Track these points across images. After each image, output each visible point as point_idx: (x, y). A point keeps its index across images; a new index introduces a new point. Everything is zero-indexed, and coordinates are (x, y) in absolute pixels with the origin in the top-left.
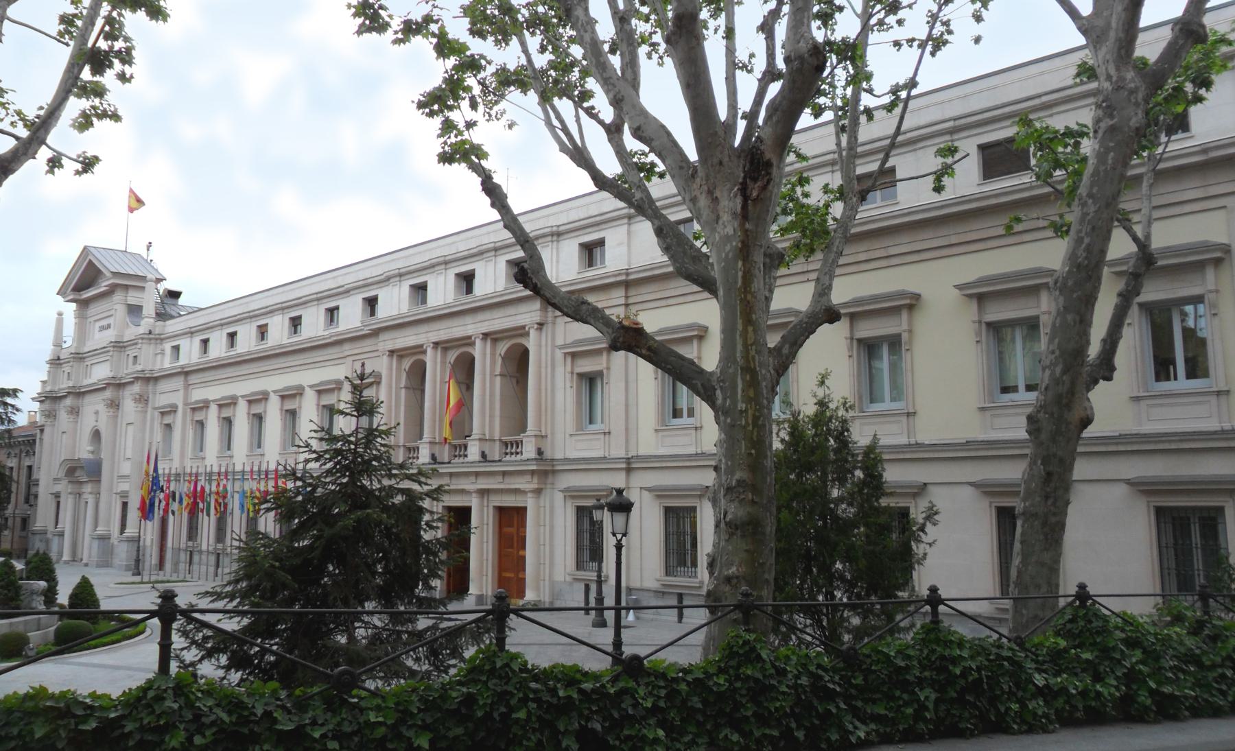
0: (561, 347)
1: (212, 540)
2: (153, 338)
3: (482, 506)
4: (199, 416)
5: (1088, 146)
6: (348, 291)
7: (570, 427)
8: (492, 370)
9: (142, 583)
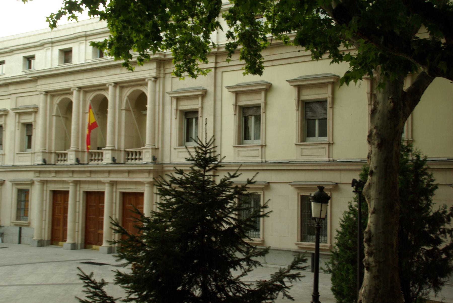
0: (169, 93)
6: (12, 51)
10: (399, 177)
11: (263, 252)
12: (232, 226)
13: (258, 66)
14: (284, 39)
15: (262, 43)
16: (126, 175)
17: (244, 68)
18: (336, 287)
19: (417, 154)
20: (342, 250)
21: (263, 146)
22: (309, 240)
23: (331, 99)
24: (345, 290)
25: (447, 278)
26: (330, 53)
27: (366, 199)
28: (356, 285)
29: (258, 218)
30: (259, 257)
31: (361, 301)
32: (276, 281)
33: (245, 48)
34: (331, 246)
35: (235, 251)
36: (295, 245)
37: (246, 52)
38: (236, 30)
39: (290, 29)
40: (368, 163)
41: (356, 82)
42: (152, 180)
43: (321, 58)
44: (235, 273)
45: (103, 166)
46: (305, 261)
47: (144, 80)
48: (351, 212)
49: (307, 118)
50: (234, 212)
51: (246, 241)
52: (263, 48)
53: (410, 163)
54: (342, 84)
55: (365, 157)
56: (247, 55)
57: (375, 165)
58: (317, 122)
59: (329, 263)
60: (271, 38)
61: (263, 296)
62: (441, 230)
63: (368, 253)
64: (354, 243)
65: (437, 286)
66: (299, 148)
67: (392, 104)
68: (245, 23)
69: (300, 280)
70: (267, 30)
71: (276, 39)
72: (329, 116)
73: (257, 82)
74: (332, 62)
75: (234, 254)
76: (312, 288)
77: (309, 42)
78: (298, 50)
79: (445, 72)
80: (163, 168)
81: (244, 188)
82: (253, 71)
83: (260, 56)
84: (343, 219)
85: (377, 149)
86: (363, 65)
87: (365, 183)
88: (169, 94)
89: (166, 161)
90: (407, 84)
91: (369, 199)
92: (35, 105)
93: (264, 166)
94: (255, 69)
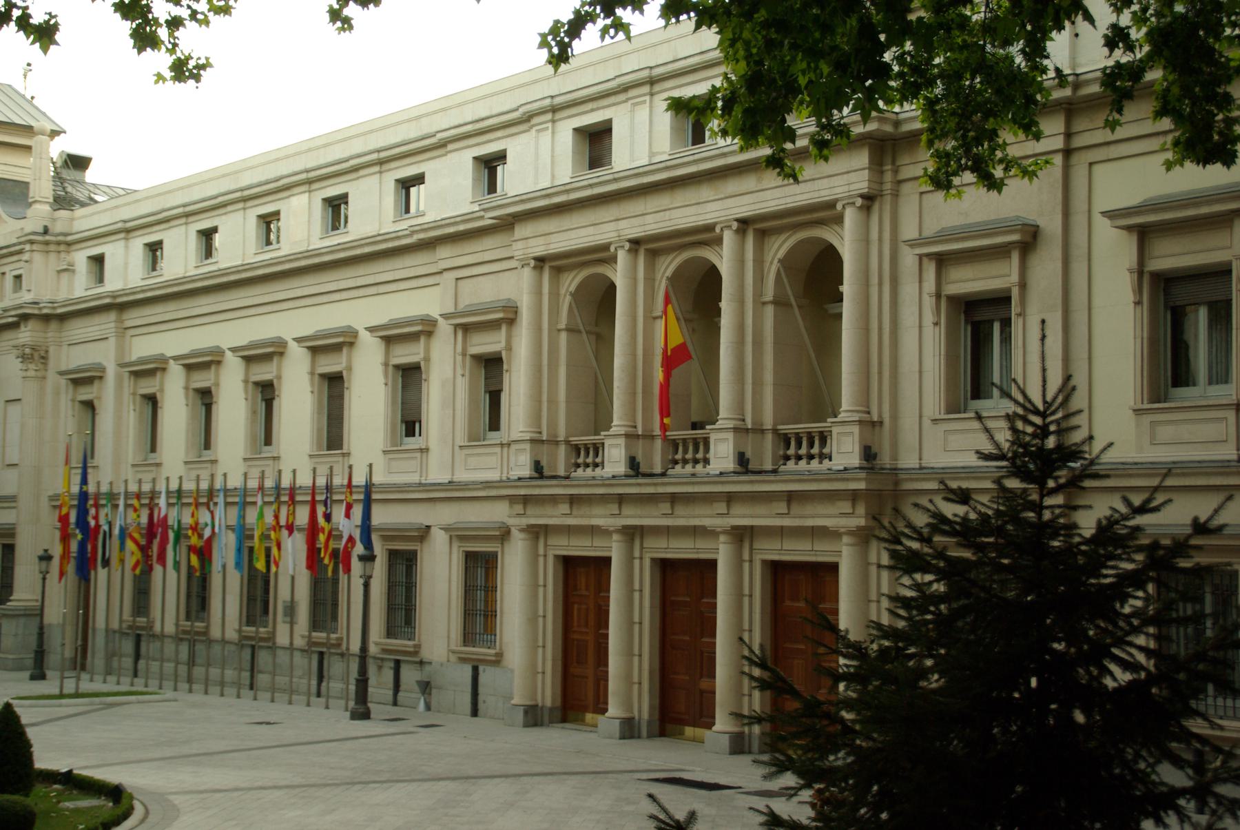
0: (912, 244)
1: (127, 615)
2: (52, 242)
3: (629, 559)
4: (147, 386)
5: (1016, 53)
6: (442, 145)
7: (934, 401)
8: (758, 293)
9: (62, 696)
13: (1220, 133)
16: (782, 507)
17: (1168, 145)
37: (1176, 90)
42: (862, 522)
45: (604, 482)
47: (831, 205)
51: (1195, 730)
56: (1179, 100)
73: (1217, 187)
75: (1154, 772)
80: (897, 483)
81: (1181, 547)
88: (912, 246)
89: (908, 460)
92: (350, 327)
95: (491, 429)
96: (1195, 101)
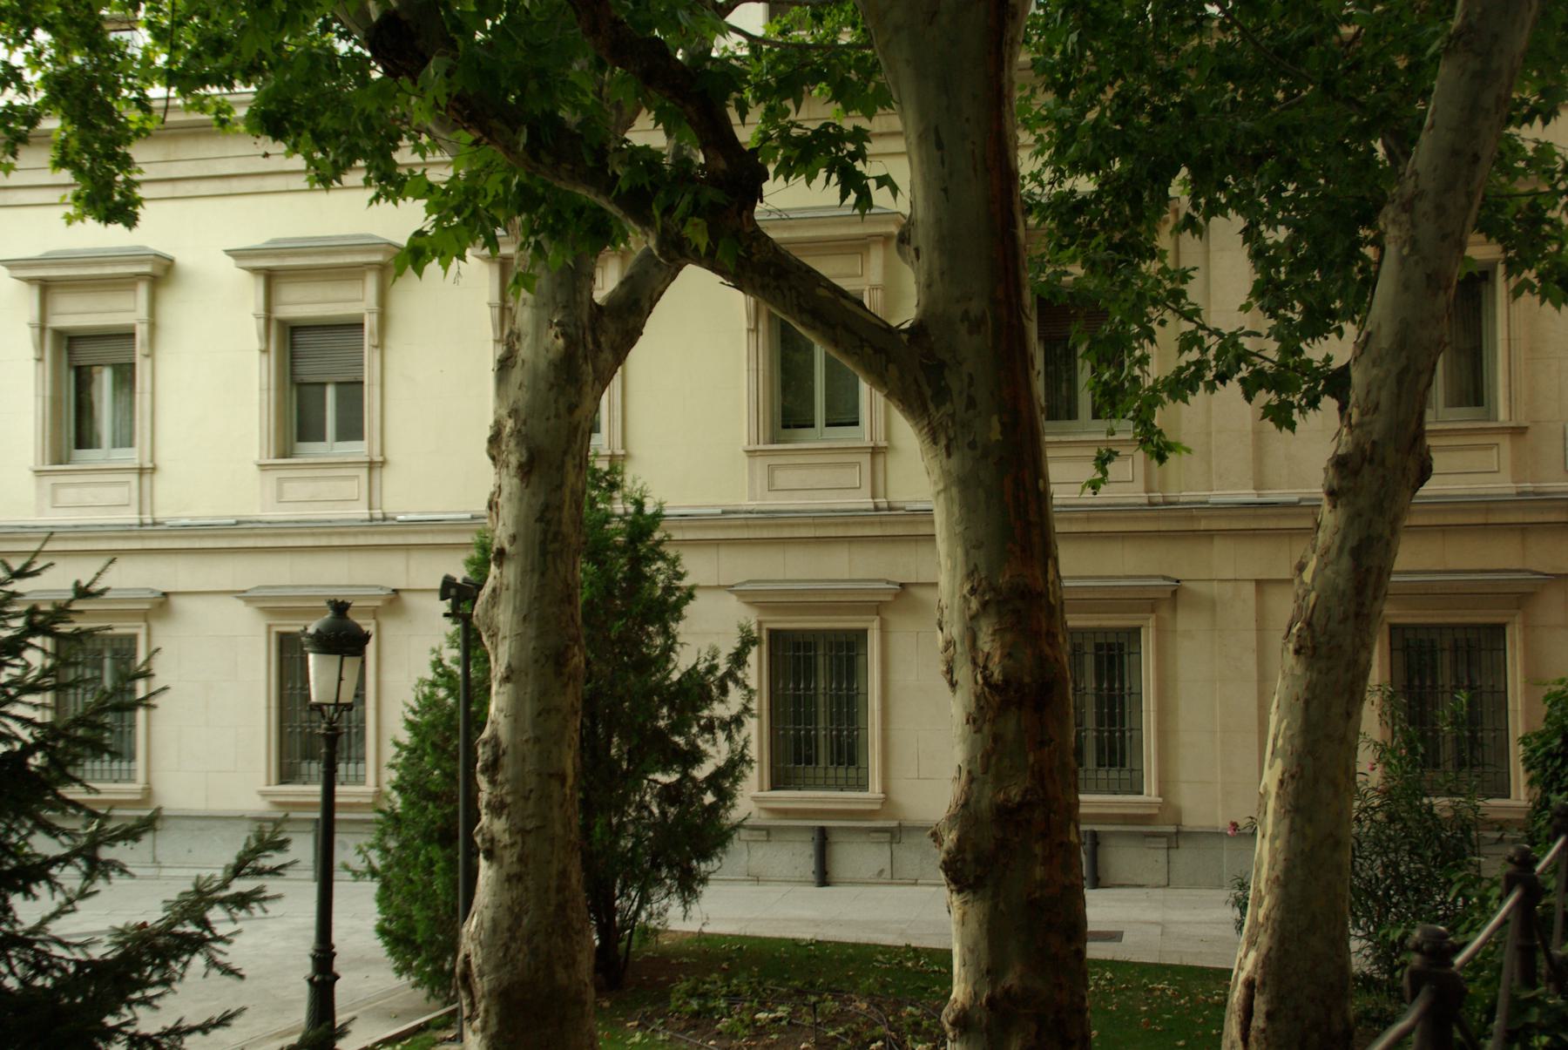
10: (585, 569)
11: (133, 827)
12: (18, 746)
13: (121, 194)
14: (214, 109)
15: (134, 115)
17: (69, 200)
18: (391, 921)
19: (637, 496)
20: (410, 804)
21: (374, 465)
22: (305, 778)
23: (374, 318)
24: (421, 927)
25: (716, 861)
26: (369, 169)
27: (485, 638)
28: (455, 910)
29: (127, 714)
30: (121, 844)
31: (467, 956)
32: (180, 921)
33: (69, 129)
34: (379, 794)
35: (31, 833)
36: (258, 798)
37: (74, 143)
38: (35, 61)
39: (232, 78)
40: (490, 525)
41: (446, 267)
43: (340, 182)
44: (27, 911)
46: (281, 846)
48: (440, 681)
49: (298, 379)
50: (27, 698)
51: (70, 797)
52: (137, 134)
53: (615, 524)
54: (400, 273)
55: (481, 507)
56: (78, 153)
57: (511, 531)
58: (330, 393)
59: (372, 847)
60: (163, 103)
61: (135, 975)
62: (702, 722)
63: (488, 805)
64: (450, 776)
65: (689, 885)
66: (273, 476)
67: (561, 342)
68: (66, 40)
69: (265, 911)
70: (148, 73)
71: (188, 108)
72: (370, 375)
73: (120, 249)
74: (377, 198)
75: (27, 844)
76: (312, 934)
77: (298, 128)
78: (262, 152)
79: (703, 250)
81: (62, 612)
82: (103, 213)
83: (126, 162)
84: (415, 705)
85: (516, 481)
86: (467, 213)
87: (480, 587)
90: (607, 281)
91: (493, 636)
93: (154, 538)
94: (110, 205)
95: (302, 437)
96: (94, 158)
